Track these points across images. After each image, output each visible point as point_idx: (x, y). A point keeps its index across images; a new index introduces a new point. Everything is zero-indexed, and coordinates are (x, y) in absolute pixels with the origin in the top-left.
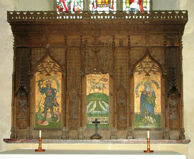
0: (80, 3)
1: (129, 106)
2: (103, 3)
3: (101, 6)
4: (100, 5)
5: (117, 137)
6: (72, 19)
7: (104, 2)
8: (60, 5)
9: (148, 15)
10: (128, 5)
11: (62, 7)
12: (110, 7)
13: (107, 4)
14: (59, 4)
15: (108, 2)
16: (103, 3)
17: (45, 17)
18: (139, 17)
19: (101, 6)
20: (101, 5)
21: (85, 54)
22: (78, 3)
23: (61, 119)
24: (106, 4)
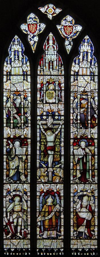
0: (26, 227)
1: (14, 252)
2: (51, 227)
3: (48, 229)
4: (48, 228)
5: (16, 99)
6: (23, 255)
7: (51, 225)
8: (7, 228)
9: (29, 251)
10: (76, 229)
11: (8, 230)
12: (57, 231)
13: (54, 228)
14: (5, 228)
15: (55, 226)
16: (51, 227)
17: (43, 253)
18: (46, 254)
19: (48, 229)
20: (49, 228)
21: (63, 26)
22: (24, 227)
23: (79, 100)
24: (53, 228)
